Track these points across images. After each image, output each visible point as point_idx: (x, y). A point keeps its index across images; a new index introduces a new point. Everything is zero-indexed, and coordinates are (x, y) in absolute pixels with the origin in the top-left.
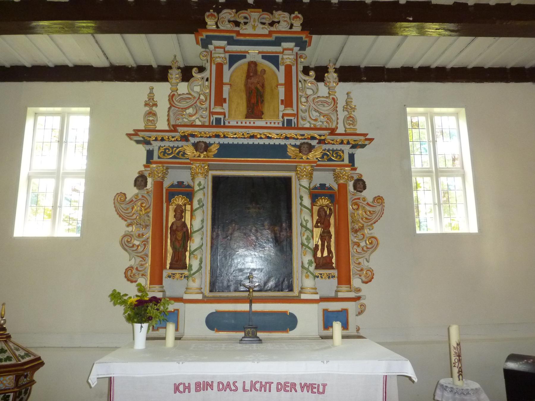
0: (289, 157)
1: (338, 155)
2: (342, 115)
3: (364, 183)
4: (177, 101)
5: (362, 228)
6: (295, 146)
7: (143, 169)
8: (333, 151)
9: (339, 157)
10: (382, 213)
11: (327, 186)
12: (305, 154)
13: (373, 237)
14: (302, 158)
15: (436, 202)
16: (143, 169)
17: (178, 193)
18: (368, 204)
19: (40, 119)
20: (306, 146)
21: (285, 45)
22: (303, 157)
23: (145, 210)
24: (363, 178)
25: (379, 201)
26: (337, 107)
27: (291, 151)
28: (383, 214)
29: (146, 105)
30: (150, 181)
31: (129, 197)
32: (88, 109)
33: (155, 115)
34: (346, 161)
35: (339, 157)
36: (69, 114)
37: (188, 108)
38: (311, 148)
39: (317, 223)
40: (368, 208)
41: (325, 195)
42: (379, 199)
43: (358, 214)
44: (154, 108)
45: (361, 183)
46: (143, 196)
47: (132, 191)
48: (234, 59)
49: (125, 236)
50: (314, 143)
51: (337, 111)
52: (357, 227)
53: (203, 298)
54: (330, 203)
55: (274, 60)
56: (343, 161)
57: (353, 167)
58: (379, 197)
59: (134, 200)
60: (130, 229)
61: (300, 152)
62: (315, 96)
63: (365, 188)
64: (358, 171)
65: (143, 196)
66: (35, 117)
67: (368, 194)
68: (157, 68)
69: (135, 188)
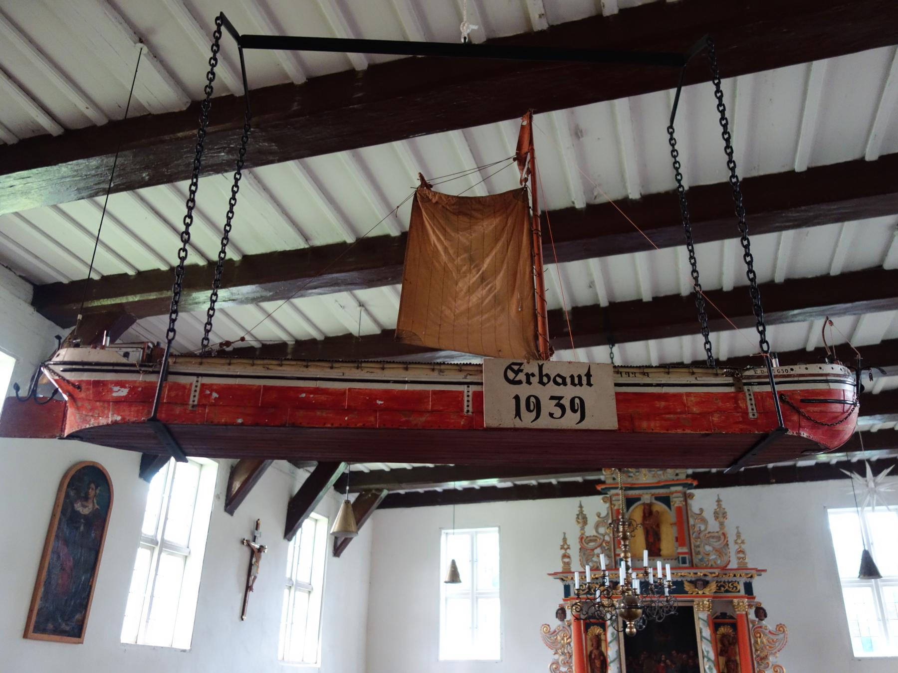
0: (686, 592)
1: (734, 587)
2: (733, 548)
3: (764, 611)
4: (585, 542)
5: (766, 657)
6: (691, 582)
7: (562, 602)
8: (729, 582)
9: (735, 589)
10: (785, 641)
11: (728, 614)
12: (700, 590)
13: (779, 666)
14: (698, 593)
15: (881, 618)
16: (562, 602)
17: (594, 624)
18: (770, 632)
19: (449, 536)
20: (701, 583)
21: (673, 489)
22: (699, 592)
23: (567, 639)
24: (763, 606)
25: (781, 629)
26: (727, 541)
27: (687, 587)
28: (786, 642)
29: (562, 548)
30: (568, 612)
31: (552, 630)
32: (497, 529)
33: (569, 557)
34: (742, 592)
35: (735, 589)
36: (477, 532)
37: (596, 548)
38: (706, 584)
39: (721, 650)
40: (771, 636)
41: (727, 624)
42: (781, 627)
43: (762, 642)
44: (568, 551)
45: (761, 611)
46: (564, 627)
47: (555, 623)
48: (630, 502)
49: (553, 664)
50: (707, 579)
51: (728, 545)
52: (762, 655)
53: (591, 580)
54: (733, 631)
55: (666, 500)
56: (739, 591)
57: (875, 505)
58: (780, 626)
59: (557, 631)
60: (556, 657)
61: (696, 587)
62: (707, 532)
63: (765, 616)
64: (756, 600)
65: (564, 627)
66: (14, 134)
67: (769, 623)
68: (557, 485)
69: (557, 619)
